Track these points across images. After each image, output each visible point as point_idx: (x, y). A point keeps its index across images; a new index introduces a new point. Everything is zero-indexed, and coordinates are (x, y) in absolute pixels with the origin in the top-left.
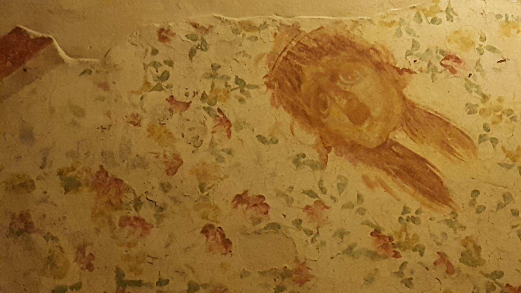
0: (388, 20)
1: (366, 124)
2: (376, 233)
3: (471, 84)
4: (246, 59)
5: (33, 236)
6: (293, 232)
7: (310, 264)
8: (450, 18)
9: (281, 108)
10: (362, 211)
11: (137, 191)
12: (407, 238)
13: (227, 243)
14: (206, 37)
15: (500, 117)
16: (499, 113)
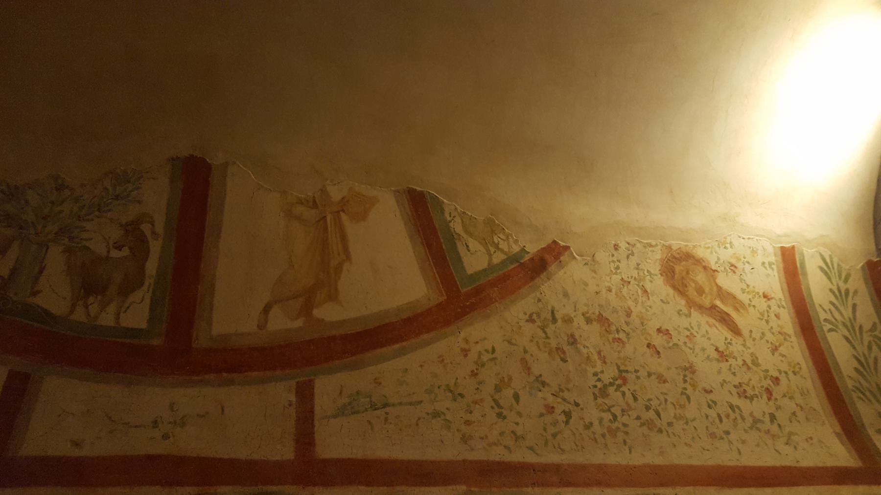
0: (707, 246)
1: (704, 296)
2: (717, 350)
3: (742, 279)
4: (650, 261)
5: (578, 345)
6: (684, 348)
7: (694, 364)
8: (731, 247)
9: (668, 286)
10: (709, 339)
11: (616, 325)
12: (729, 353)
13: (658, 353)
14: (633, 249)
15: (755, 295)
16: (754, 294)
